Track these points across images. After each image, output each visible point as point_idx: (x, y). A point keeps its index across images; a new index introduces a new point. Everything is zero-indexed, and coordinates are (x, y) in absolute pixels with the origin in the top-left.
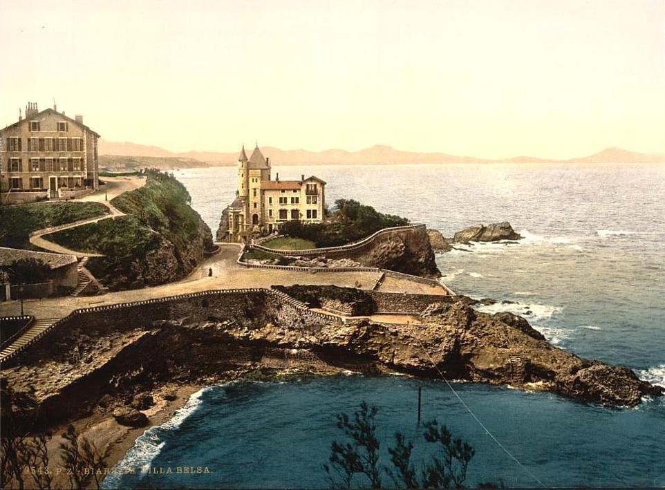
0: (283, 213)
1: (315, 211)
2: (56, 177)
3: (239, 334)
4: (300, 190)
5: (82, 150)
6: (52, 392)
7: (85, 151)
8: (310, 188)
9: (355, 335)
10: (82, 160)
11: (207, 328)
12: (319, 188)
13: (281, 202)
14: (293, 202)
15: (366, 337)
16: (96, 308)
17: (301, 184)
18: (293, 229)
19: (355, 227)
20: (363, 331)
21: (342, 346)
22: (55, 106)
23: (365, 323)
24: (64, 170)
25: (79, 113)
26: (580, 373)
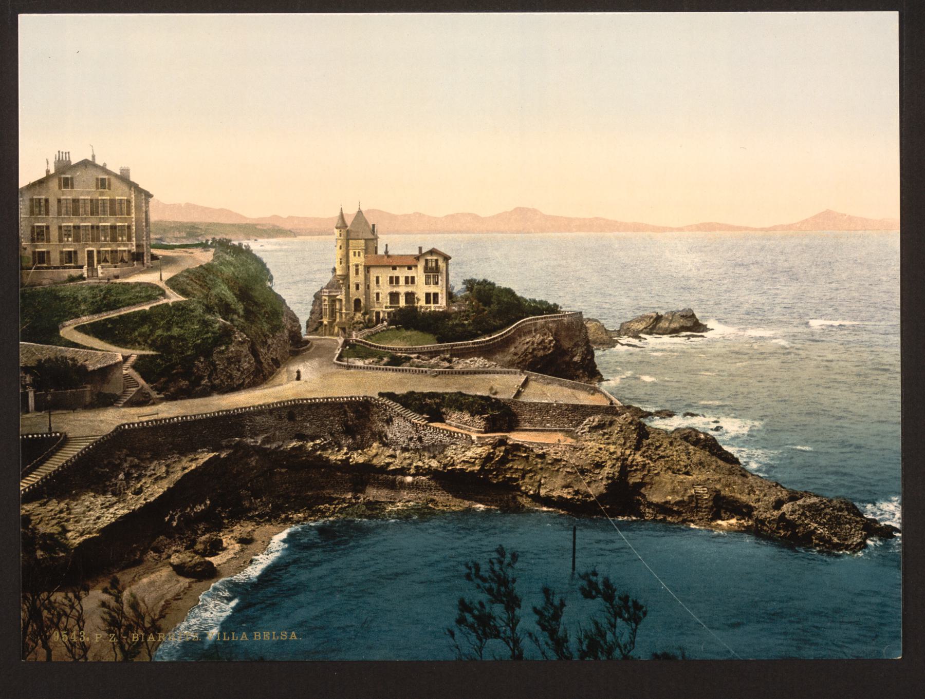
0: (394, 297)
1: (436, 295)
2: (95, 250)
3: (336, 456)
4: (416, 266)
5: (129, 213)
6: (90, 533)
7: (133, 215)
8: (430, 265)
9: (489, 458)
10: (129, 227)
11: (293, 448)
12: (441, 264)
13: (391, 282)
14: (407, 282)
15: (504, 460)
16: (147, 422)
17: (417, 258)
18: (408, 318)
19: (490, 315)
20: (500, 452)
21: (472, 472)
22: (93, 157)
23: (502, 442)
24: (105, 240)
25: (125, 166)
26: (786, 508)
